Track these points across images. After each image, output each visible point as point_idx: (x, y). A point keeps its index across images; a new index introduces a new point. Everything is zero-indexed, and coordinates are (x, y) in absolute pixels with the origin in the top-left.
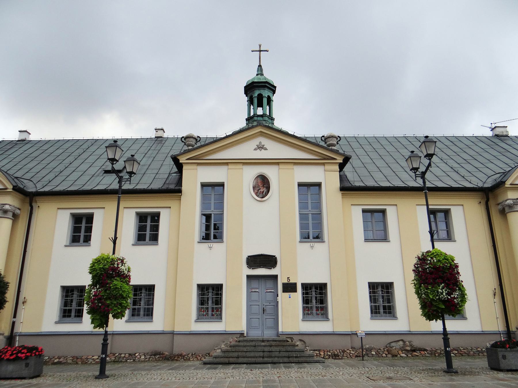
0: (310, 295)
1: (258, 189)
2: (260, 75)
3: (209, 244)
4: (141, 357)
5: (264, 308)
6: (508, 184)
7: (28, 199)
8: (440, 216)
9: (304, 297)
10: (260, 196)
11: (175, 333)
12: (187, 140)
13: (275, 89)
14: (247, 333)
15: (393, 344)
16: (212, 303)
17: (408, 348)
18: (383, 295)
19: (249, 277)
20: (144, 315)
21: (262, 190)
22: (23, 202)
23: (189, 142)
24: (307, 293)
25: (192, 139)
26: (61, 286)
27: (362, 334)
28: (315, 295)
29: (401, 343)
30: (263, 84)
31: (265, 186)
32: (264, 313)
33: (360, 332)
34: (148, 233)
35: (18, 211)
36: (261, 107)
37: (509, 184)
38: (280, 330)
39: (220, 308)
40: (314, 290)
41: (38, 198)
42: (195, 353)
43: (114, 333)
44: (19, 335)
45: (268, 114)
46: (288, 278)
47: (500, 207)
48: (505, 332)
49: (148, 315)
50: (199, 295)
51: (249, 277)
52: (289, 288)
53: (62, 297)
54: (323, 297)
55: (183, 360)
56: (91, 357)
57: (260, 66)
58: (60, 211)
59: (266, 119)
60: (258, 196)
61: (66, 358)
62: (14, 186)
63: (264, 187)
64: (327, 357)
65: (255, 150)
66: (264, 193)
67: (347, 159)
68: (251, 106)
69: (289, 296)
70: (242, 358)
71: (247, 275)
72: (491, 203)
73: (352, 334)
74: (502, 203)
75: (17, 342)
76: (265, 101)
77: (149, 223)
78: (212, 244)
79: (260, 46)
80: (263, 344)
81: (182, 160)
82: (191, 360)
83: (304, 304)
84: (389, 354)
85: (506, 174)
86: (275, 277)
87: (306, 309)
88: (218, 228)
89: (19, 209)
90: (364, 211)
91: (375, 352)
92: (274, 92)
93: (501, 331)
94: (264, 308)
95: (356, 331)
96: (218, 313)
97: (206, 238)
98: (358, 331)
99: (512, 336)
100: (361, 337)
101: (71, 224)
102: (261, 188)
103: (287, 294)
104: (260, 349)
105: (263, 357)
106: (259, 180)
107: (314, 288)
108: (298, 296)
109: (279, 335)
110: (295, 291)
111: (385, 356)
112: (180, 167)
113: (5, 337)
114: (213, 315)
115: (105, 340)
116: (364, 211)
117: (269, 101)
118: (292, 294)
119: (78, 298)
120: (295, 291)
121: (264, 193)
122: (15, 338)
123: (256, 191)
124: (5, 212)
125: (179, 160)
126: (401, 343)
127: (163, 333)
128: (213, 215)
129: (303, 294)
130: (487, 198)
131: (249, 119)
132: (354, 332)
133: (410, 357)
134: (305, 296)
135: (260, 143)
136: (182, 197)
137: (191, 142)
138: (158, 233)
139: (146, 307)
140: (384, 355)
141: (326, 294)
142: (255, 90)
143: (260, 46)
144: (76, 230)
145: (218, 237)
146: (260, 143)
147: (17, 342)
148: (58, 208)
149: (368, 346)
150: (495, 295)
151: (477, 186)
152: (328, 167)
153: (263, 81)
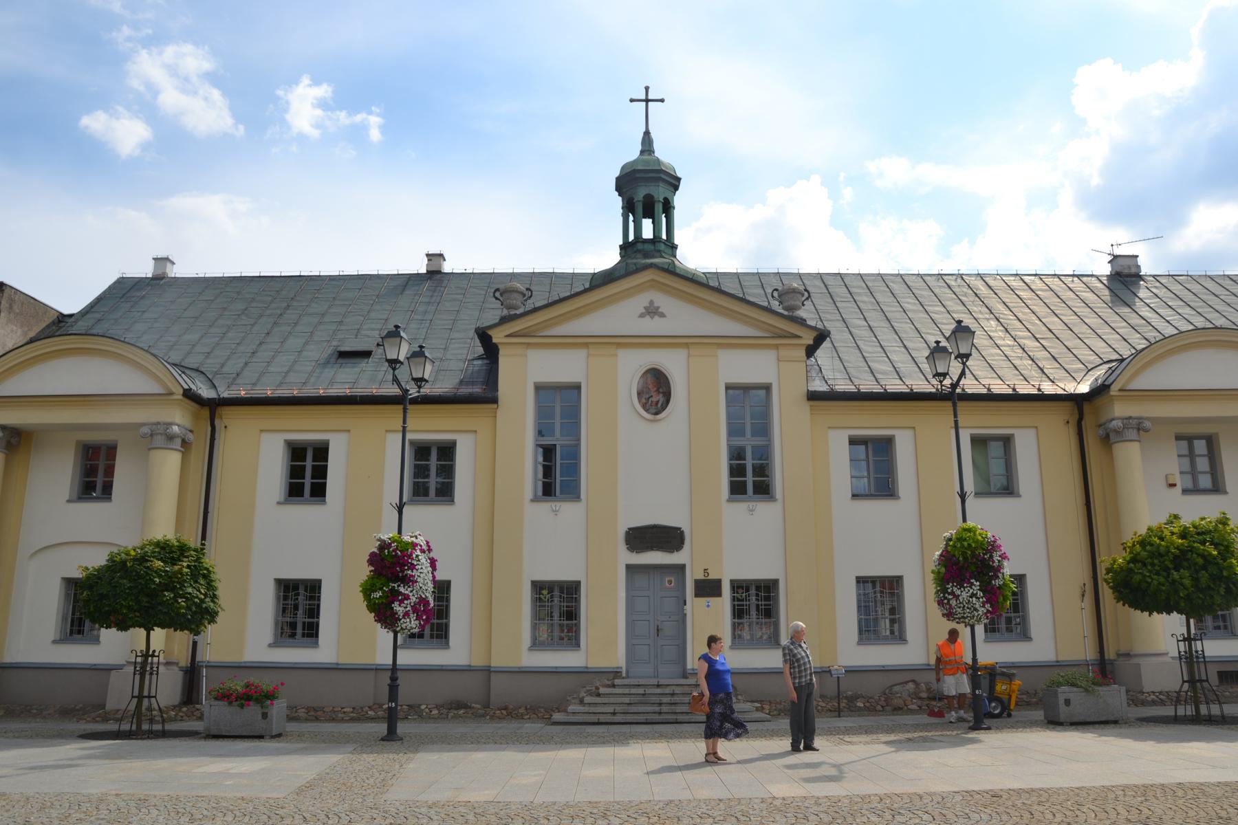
0: (746, 601)
1: (648, 396)
2: (648, 152)
3: (553, 504)
4: (431, 711)
5: (658, 626)
6: (1114, 390)
7: (206, 412)
8: (996, 449)
9: (734, 605)
10: (651, 410)
11: (492, 669)
12: (506, 295)
13: (677, 184)
14: (627, 672)
15: (896, 688)
16: (560, 617)
17: (924, 695)
18: (882, 599)
19: (630, 568)
20: (432, 636)
21: (654, 399)
22: (196, 417)
23: (511, 302)
25: (516, 295)
26: (275, 579)
27: (840, 672)
28: (756, 602)
29: (911, 685)
31: (661, 390)
32: (658, 635)
33: (836, 667)
34: (308, 481)
35: (190, 436)
36: (649, 218)
37: (1117, 389)
39: (576, 624)
41: (226, 412)
42: (531, 707)
43: (378, 667)
44: (206, 666)
45: (664, 237)
46: (705, 570)
47: (1101, 432)
48: (1096, 662)
49: (439, 637)
51: (630, 568)
52: (708, 588)
53: (278, 598)
54: (770, 605)
55: (510, 717)
56: (340, 709)
57: (647, 133)
58: (265, 436)
59: (662, 247)
60: (647, 411)
61: (295, 709)
62: (185, 390)
63: (659, 392)
64: (775, 713)
65: (642, 316)
66: (659, 405)
67: (822, 337)
68: (629, 216)
69: (707, 604)
70: (622, 715)
71: (627, 565)
72: (1088, 423)
73: (823, 671)
74: (1105, 424)
75: (204, 678)
76: (659, 208)
77: (433, 462)
78: (558, 504)
79: (647, 89)
80: (659, 691)
81: (497, 336)
82: (526, 717)
83: (734, 618)
84: (887, 705)
85: (1114, 370)
86: (681, 568)
87: (738, 628)
88: (763, 470)
89: (191, 431)
90: (853, 441)
91: (864, 703)
92: (676, 188)
93: (1090, 660)
94: (658, 626)
95: (829, 667)
96: (570, 634)
97: (548, 491)
98: (833, 666)
99: (1109, 668)
100: (838, 677)
101: (455, 464)
102: (652, 394)
103: (702, 601)
104: (653, 699)
105: (660, 704)
107: (754, 588)
108: (724, 603)
109: (688, 675)
110: (719, 594)
111: (881, 709)
112: (491, 351)
113: (181, 669)
114: (562, 639)
115: (394, 679)
116: (853, 441)
117: (668, 208)
119: (308, 602)
120: (719, 594)
121: (659, 405)
122: (199, 673)
123: (644, 401)
124: (171, 438)
125: (490, 337)
127: (467, 669)
128: (558, 448)
129: (734, 599)
130: (1079, 414)
131: (626, 248)
132: (826, 667)
133: (924, 709)
134: (736, 603)
135: (651, 302)
136: (498, 410)
137: (514, 301)
138: (451, 482)
139: (307, 620)
140: (879, 708)
141: (776, 599)
142: (638, 186)
143: (647, 89)
144: (295, 472)
145: (572, 492)
146: (651, 302)
147: (204, 678)
148: (261, 431)
149: (850, 693)
150: (1083, 595)
151: (1064, 390)
152: (784, 353)
153: (654, 168)
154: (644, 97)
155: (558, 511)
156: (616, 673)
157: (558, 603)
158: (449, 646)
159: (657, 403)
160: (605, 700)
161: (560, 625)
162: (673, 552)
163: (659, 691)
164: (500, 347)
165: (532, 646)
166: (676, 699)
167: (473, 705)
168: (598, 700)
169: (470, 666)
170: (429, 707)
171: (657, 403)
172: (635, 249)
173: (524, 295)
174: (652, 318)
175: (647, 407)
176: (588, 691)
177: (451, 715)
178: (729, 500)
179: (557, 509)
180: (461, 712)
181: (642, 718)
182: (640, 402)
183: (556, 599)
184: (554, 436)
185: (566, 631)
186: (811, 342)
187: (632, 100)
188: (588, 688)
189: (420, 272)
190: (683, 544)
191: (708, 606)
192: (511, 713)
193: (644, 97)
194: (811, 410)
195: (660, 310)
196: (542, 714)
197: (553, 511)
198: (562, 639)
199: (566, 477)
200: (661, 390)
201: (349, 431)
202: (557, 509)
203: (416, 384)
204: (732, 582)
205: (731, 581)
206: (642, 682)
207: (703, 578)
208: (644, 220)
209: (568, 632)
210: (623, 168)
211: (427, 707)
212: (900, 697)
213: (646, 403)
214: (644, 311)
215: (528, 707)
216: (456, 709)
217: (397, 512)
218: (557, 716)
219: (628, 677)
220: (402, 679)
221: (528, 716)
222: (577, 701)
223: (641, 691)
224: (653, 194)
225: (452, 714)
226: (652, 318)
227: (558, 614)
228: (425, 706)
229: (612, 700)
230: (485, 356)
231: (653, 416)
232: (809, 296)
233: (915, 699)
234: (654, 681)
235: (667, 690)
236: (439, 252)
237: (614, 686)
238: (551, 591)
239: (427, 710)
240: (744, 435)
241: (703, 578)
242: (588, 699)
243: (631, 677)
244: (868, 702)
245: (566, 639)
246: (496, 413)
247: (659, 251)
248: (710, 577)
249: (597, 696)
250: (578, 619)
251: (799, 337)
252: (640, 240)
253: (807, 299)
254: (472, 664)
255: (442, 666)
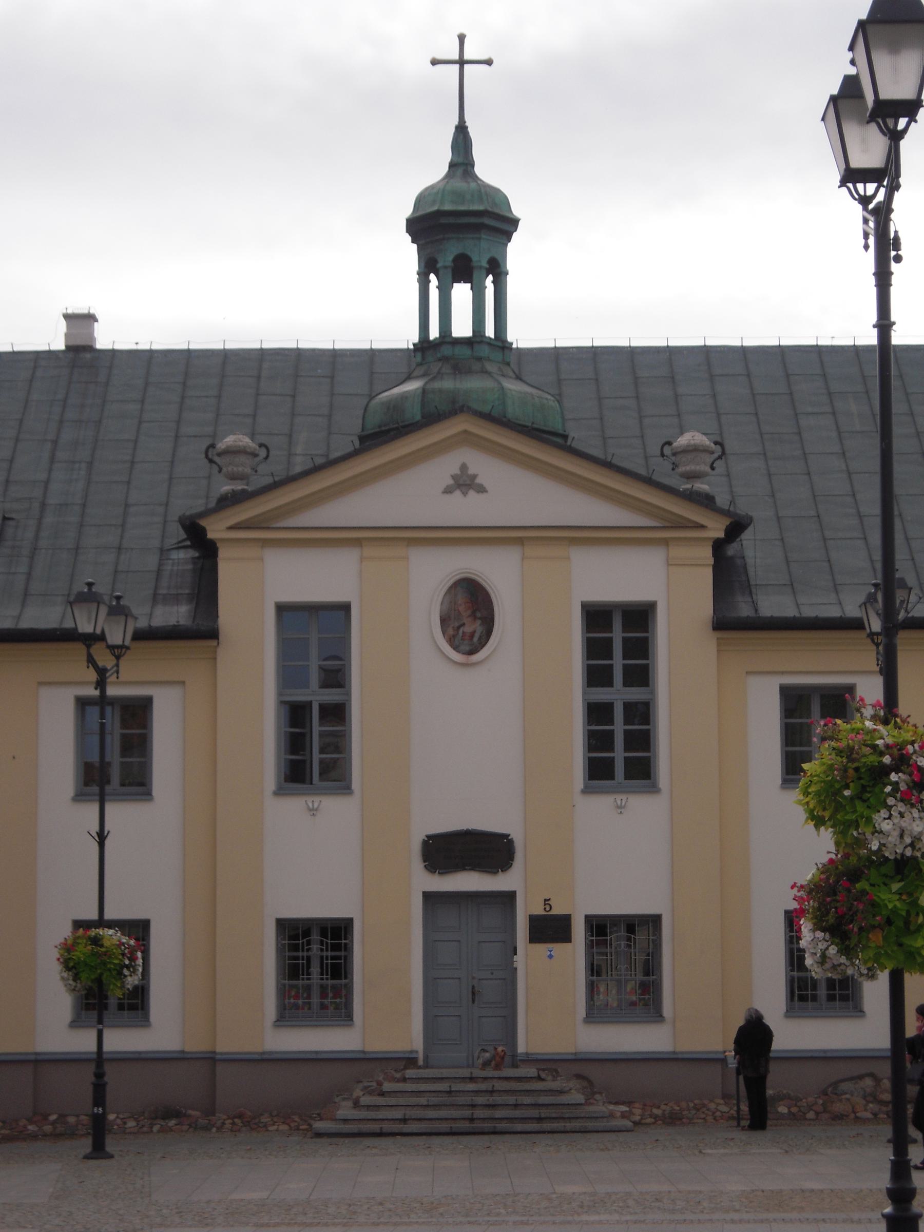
1: (457, 624)
3: (309, 799)
5: (473, 987)
11: (218, 1057)
14: (426, 1058)
15: (844, 1086)
16: (322, 974)
19: (430, 898)
21: (468, 629)
24: (295, 948)
29: (869, 1082)
30: (473, 220)
32: (473, 1001)
38: (521, 1048)
39: (346, 985)
40: (315, 937)
46: (545, 900)
50: (280, 950)
51: (430, 898)
57: (462, 131)
58: (45, 692)
60: (456, 648)
65: (448, 491)
66: (475, 639)
78: (317, 799)
81: (215, 529)
86: (509, 898)
91: (789, 1108)
94: (473, 987)
103: (542, 949)
104: (461, 1100)
106: (461, 598)
114: (323, 1007)
115: (99, 1075)
117: (497, 269)
118: (558, 949)
121: (475, 639)
125: (203, 531)
126: (869, 1082)
135: (464, 467)
140: (811, 1115)
141: (348, 948)
143: (462, 38)
146: (464, 467)
152: (680, 552)
154: (467, 57)
155: (316, 810)
156: (410, 1061)
157: (319, 953)
158: (862, 1011)
159: (472, 635)
160: (392, 1101)
161: (322, 986)
162: (496, 873)
163: (471, 1086)
164: (218, 545)
165: (278, 1020)
166: (498, 1099)
167: (190, 1112)
168: (381, 1101)
169: (183, 1052)
170: (121, 1116)
171: (472, 635)
172: (439, 355)
173: (255, 455)
174: (465, 494)
175: (457, 642)
176: (365, 1088)
177: (156, 1128)
178: (586, 791)
179: (316, 806)
180: (172, 1123)
181: (444, 1126)
182: (444, 633)
183: (315, 947)
184: (308, 688)
185: (330, 995)
186: (721, 535)
187: (435, 62)
188: (366, 1084)
189: (53, 348)
190: (513, 860)
191: (551, 957)
192: (249, 1122)
193: (457, 67)
194: (718, 645)
195: (478, 481)
196: (296, 1124)
197: (310, 810)
198: (323, 1007)
199: (342, 932)
200: (478, 615)
201: (183, 683)
202: (316, 806)
203: (114, 654)
204: (588, 919)
205: (586, 917)
206: (445, 1073)
207: (544, 913)
208: (456, 286)
209: (334, 997)
210: (420, 201)
211: (117, 1117)
212: (848, 1100)
213: (454, 636)
214: (451, 482)
215: (275, 1113)
216: (163, 1119)
217: (96, 844)
218: (319, 1125)
219: (426, 1066)
220: (111, 1075)
221: (275, 1127)
222: (350, 1104)
223: (443, 1086)
224: (469, 253)
225: (158, 1126)
226: (465, 494)
227: (319, 970)
228: (115, 1115)
229: (402, 1101)
230: (188, 543)
231: (466, 656)
232: (723, 453)
233: (872, 1102)
234: (465, 1073)
235: (483, 1086)
236: (86, 311)
237: (404, 1080)
238: (307, 933)
239: (119, 1121)
240: (610, 684)
241: (543, 913)
242: (366, 1100)
243: (432, 1067)
244: (796, 1105)
245: (331, 1008)
246: (215, 652)
247: (480, 359)
248: (554, 912)
249: (379, 1095)
250: (349, 976)
251: (702, 527)
252: (448, 339)
253: (720, 458)
254: (187, 1050)
255: (140, 1053)
